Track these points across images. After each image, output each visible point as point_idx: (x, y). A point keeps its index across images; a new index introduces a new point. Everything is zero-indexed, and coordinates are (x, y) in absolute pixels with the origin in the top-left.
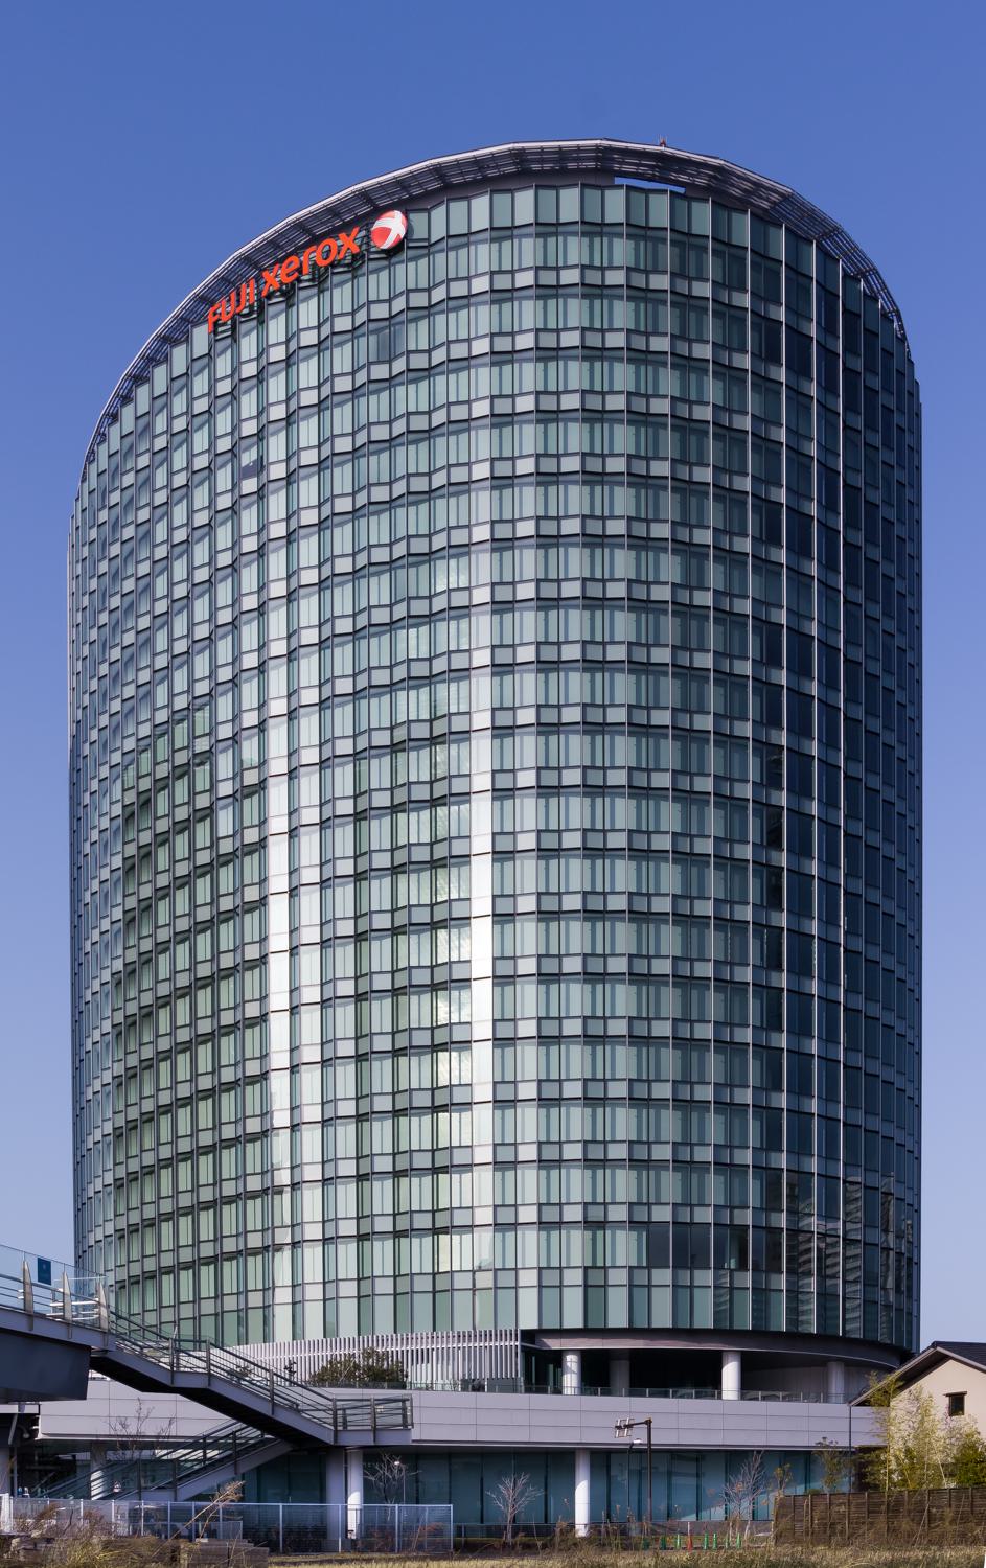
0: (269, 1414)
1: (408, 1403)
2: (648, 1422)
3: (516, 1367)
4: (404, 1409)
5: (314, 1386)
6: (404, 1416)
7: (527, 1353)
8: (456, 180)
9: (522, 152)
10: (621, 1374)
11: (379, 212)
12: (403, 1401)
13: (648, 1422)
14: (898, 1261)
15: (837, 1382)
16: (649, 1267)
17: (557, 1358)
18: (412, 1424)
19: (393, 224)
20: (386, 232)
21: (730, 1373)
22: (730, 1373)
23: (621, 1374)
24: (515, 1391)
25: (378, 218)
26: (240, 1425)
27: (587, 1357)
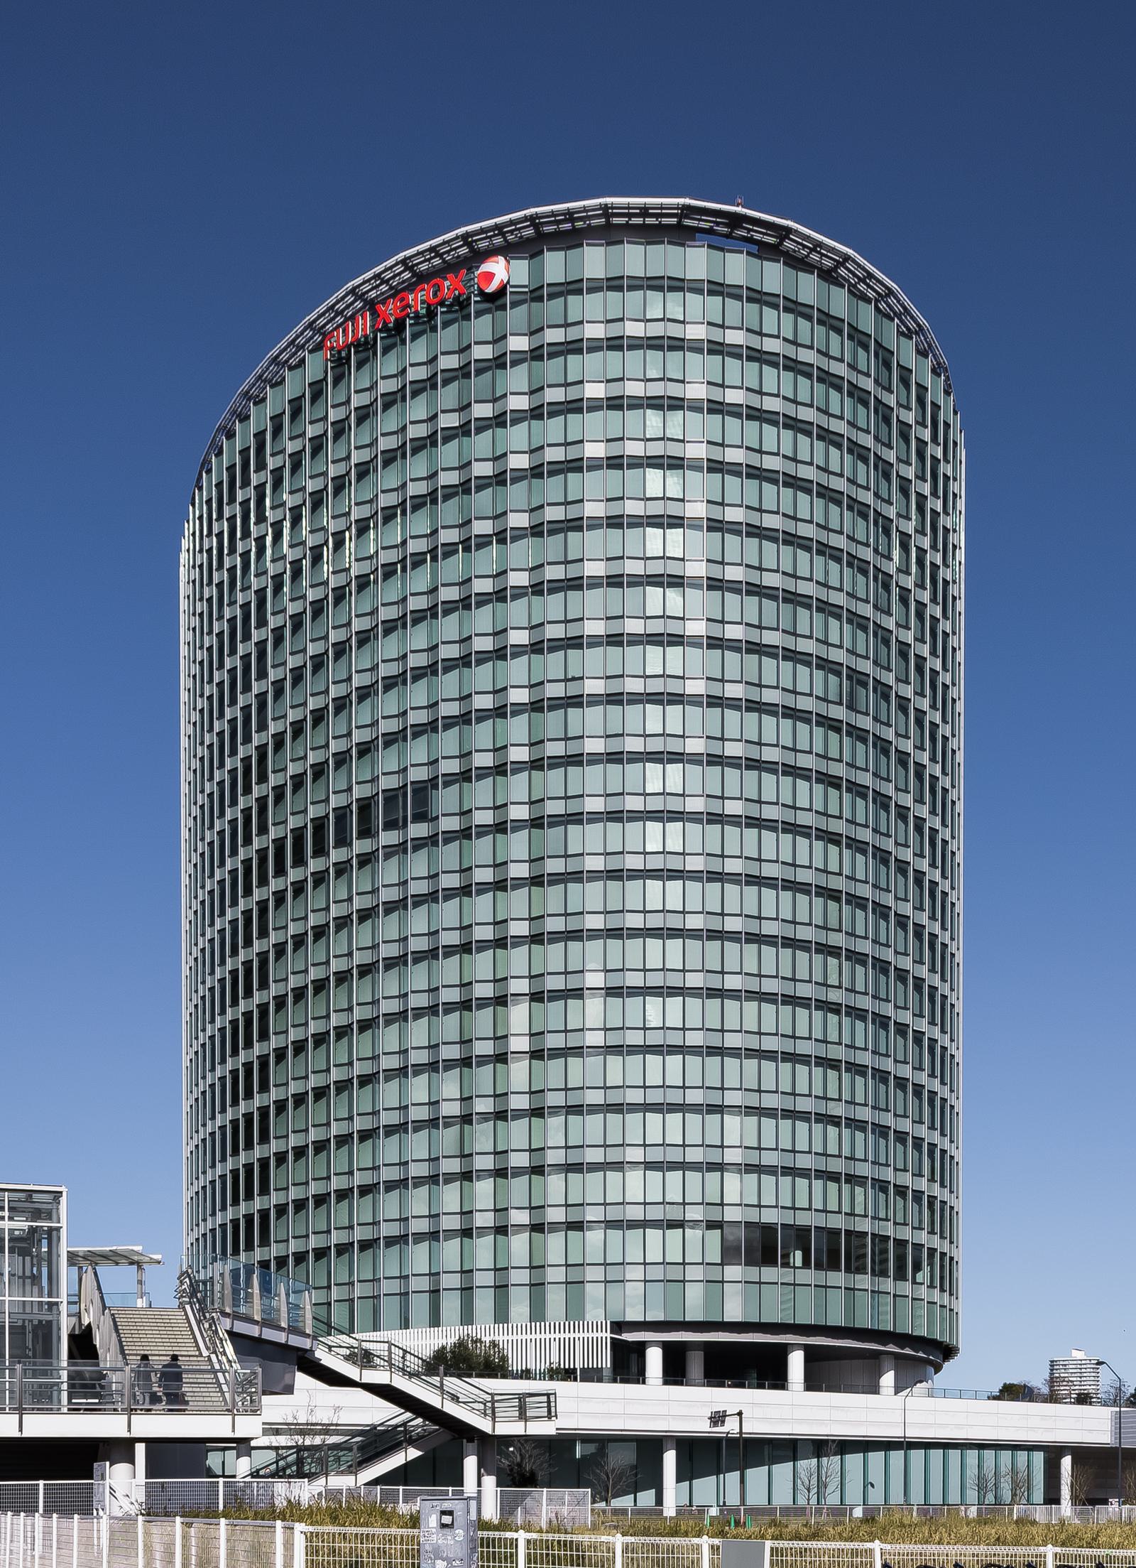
0: (439, 1407)
1: (552, 1398)
2: (740, 1414)
3: (606, 1361)
4: (549, 1402)
5: (426, 1375)
6: (549, 1407)
7: (616, 1345)
8: (483, 245)
9: (537, 216)
10: (696, 1365)
11: (482, 256)
12: (548, 1395)
13: (740, 1414)
14: (942, 1259)
15: (888, 1379)
16: (722, 1264)
17: (641, 1348)
18: (556, 1416)
19: (499, 270)
20: (490, 276)
21: (796, 1362)
22: (796, 1362)
23: (696, 1365)
24: (600, 1380)
25: (482, 263)
26: (408, 1415)
27: (668, 1348)
